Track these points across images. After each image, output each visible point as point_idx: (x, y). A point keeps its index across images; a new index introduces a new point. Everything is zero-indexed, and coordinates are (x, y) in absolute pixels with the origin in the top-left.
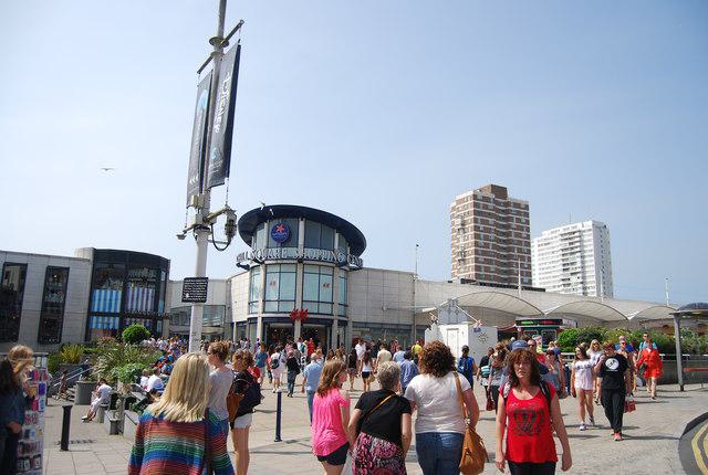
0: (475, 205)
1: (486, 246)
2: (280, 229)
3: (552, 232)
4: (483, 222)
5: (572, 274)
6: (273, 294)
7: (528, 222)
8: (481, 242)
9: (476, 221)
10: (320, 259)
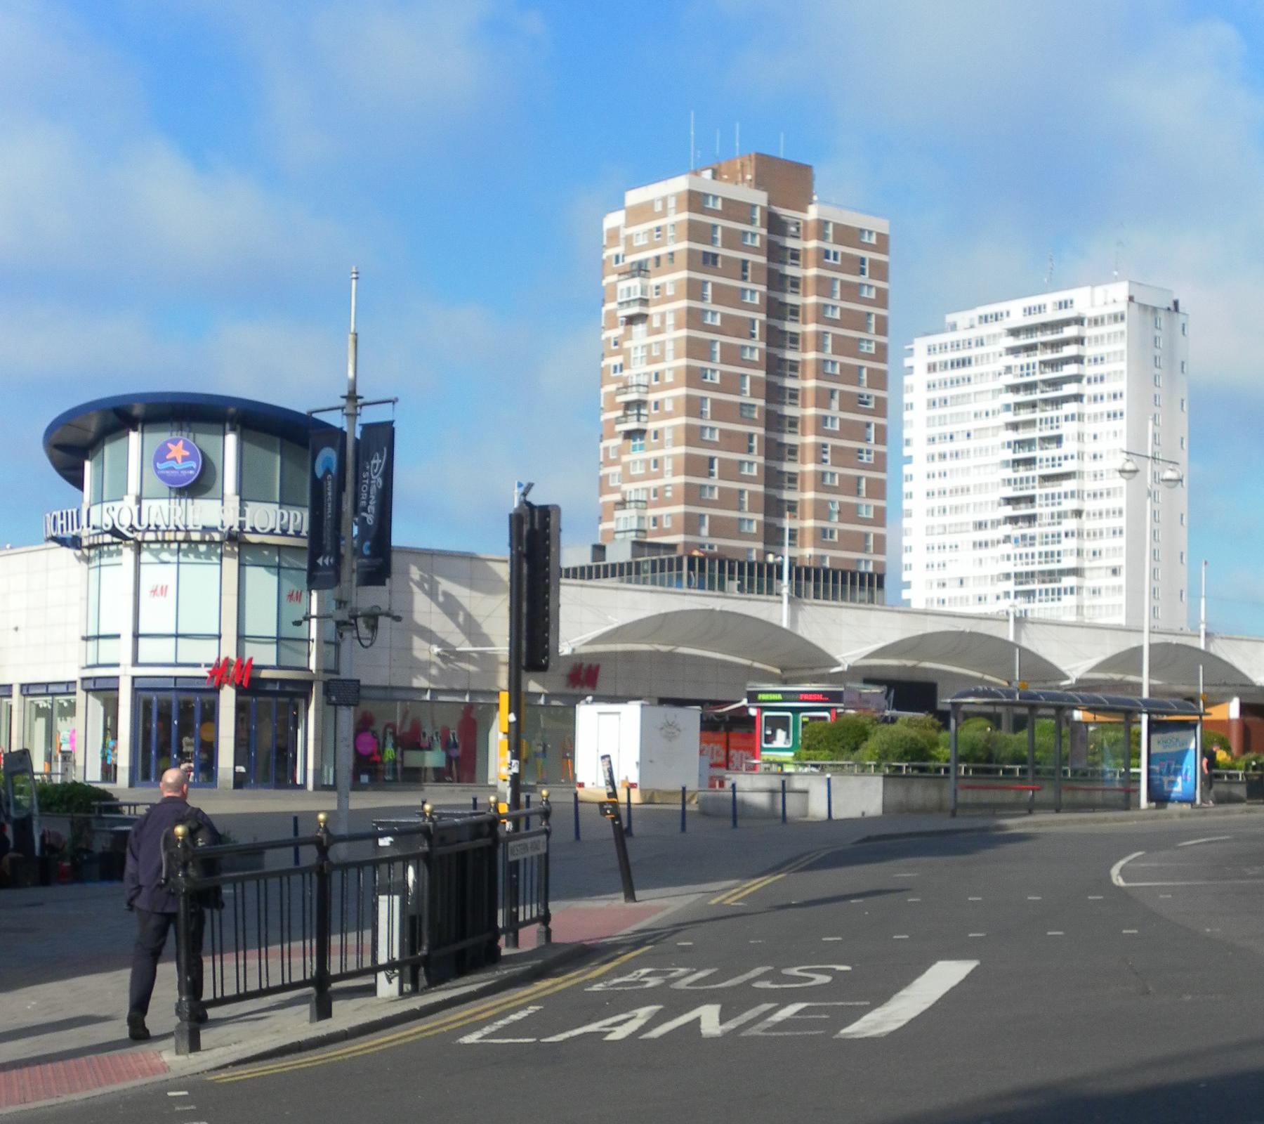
0: (695, 231)
1: (731, 384)
2: (178, 451)
3: (985, 319)
4: (722, 295)
5: (1046, 478)
6: (156, 617)
7: (882, 299)
8: (717, 368)
9: (694, 290)
10: (284, 533)
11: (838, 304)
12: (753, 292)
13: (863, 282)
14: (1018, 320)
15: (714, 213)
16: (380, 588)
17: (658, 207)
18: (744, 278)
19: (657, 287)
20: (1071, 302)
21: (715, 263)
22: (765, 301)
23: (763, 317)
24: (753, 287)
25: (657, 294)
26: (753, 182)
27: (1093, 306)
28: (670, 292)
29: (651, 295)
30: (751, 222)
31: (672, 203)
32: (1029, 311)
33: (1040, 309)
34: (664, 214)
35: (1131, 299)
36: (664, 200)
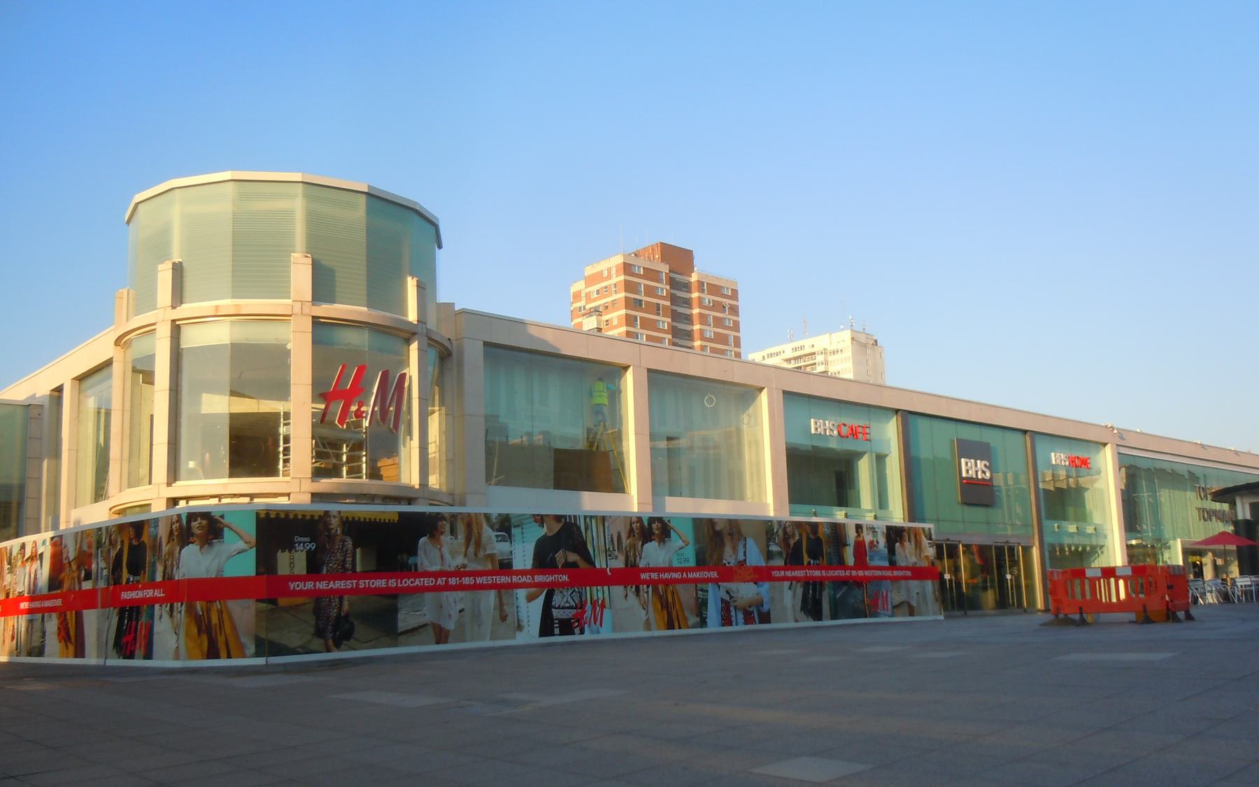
0: (629, 286)
4: (646, 324)
7: (736, 327)
11: (710, 332)
12: (663, 322)
13: (725, 317)
14: (789, 354)
15: (638, 276)
16: (740, 323)
17: (605, 274)
18: (658, 314)
19: (607, 321)
20: (804, 346)
21: (641, 305)
22: (670, 328)
23: (670, 337)
24: (664, 319)
25: (607, 325)
26: (660, 259)
27: (831, 344)
28: (615, 322)
29: (603, 326)
30: (659, 281)
31: (614, 271)
32: (795, 349)
33: (802, 348)
34: (609, 277)
35: (853, 339)
36: (609, 270)
